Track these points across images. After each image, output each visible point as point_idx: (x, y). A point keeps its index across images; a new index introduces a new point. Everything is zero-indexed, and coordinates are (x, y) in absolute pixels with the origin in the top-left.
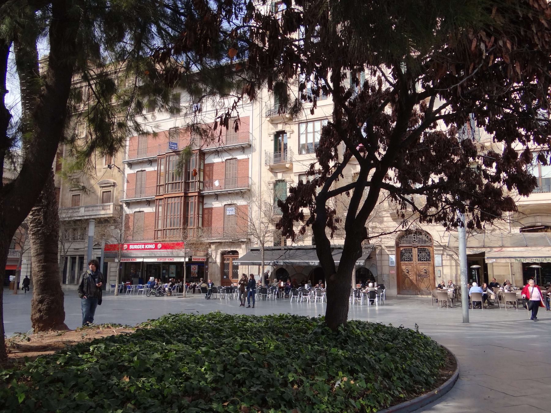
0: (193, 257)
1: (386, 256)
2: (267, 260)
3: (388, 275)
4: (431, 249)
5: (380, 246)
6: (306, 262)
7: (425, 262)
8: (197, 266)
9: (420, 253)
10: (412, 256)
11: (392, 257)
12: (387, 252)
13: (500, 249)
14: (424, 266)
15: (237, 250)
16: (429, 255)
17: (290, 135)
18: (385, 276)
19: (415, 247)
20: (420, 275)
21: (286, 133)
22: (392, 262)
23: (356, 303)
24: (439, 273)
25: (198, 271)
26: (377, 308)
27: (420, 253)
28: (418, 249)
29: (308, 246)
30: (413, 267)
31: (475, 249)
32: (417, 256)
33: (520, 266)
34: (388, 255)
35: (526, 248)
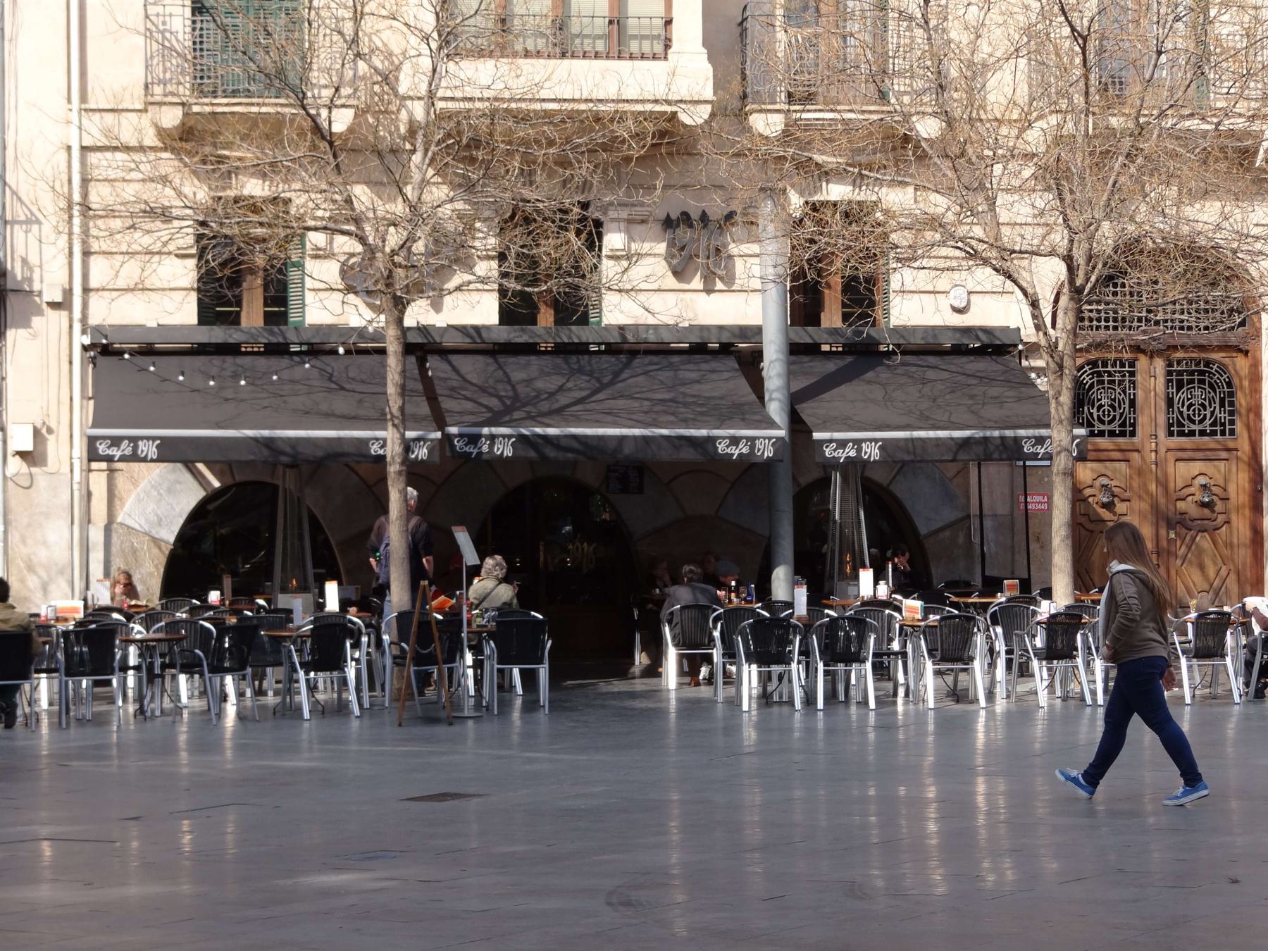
4: (1241, 363)
6: (690, 440)
10: (1133, 403)
14: (1197, 467)
16: (1228, 400)
19: (1152, 355)
20: (1178, 522)
23: (765, 698)
27: (1180, 386)
29: (914, 329)
32: (1162, 404)
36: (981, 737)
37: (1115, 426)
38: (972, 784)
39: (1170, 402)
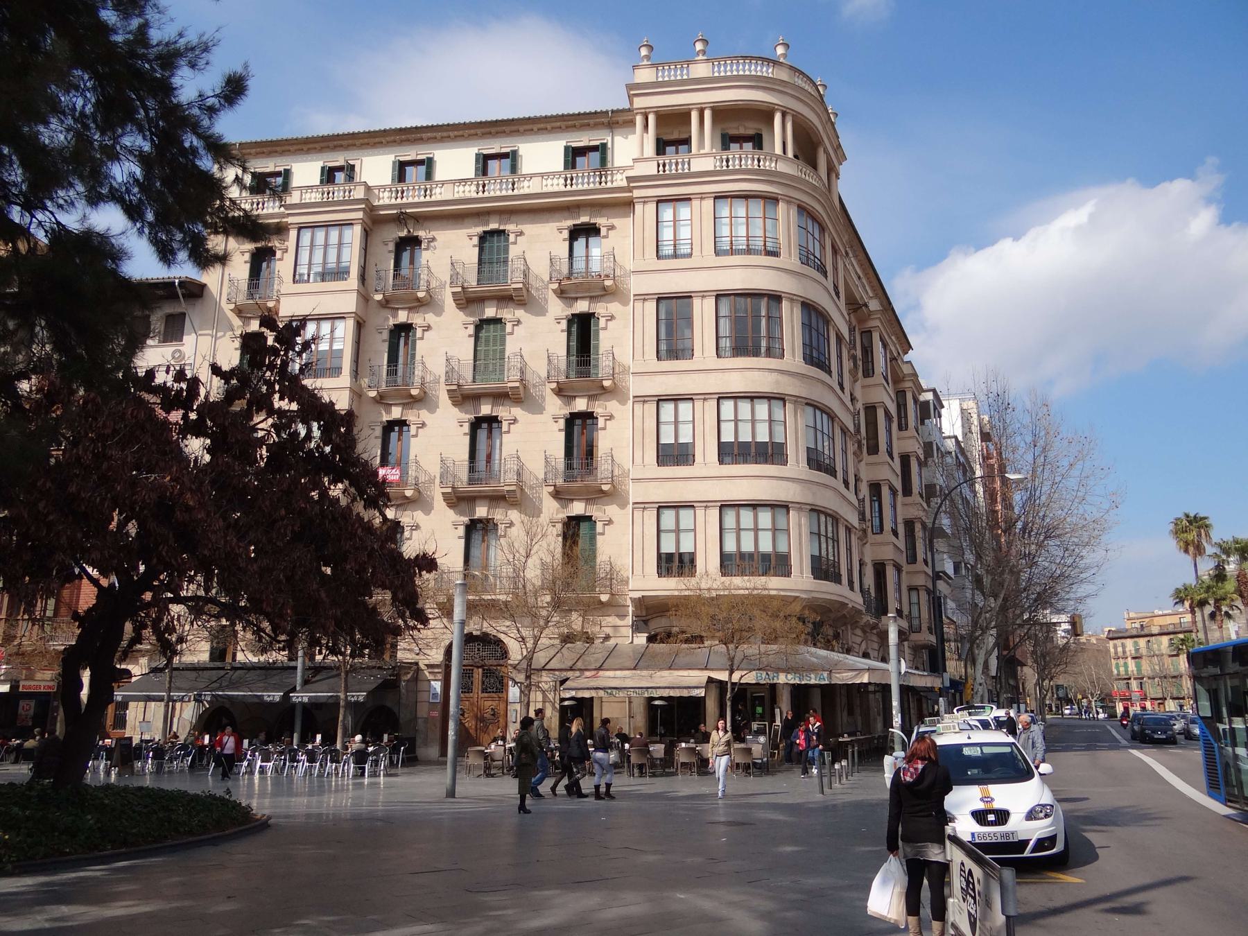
0: (21, 683)
1: (426, 683)
2: (179, 689)
3: (426, 720)
5: (417, 664)
7: (494, 695)
8: (33, 703)
9: (487, 677)
10: (472, 683)
11: (435, 686)
12: (427, 674)
13: (593, 673)
14: (490, 703)
15: (130, 667)
17: (417, 432)
18: (420, 721)
19: (478, 667)
21: (409, 426)
22: (435, 695)
24: (514, 715)
25: (35, 714)
26: (366, 781)
27: (487, 677)
28: (484, 670)
30: (472, 704)
31: (557, 673)
33: (642, 701)
34: (429, 681)
35: (634, 671)
36: (257, 788)
37: (494, 690)
38: (272, 790)
39: (483, 683)
